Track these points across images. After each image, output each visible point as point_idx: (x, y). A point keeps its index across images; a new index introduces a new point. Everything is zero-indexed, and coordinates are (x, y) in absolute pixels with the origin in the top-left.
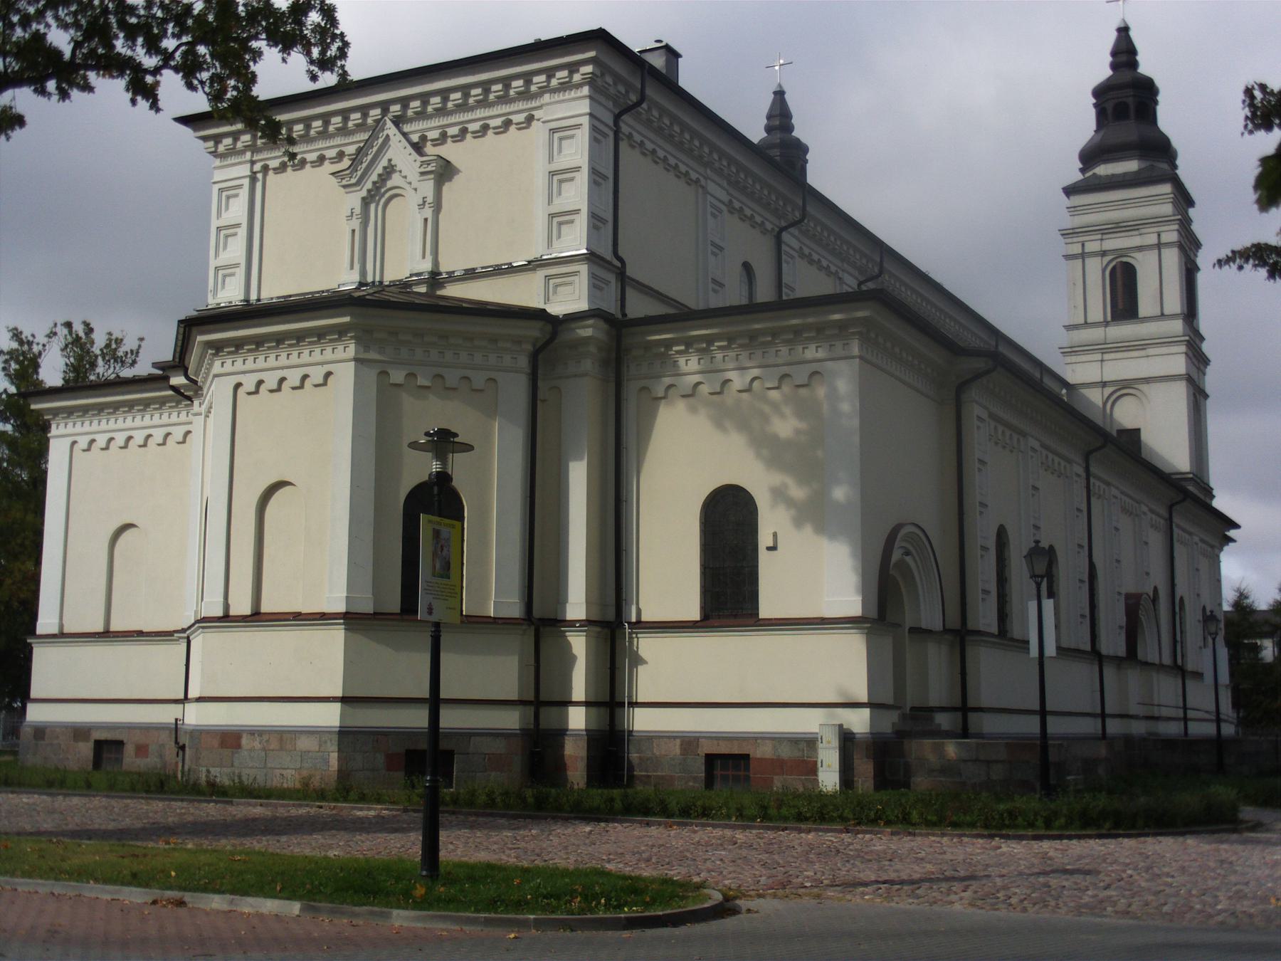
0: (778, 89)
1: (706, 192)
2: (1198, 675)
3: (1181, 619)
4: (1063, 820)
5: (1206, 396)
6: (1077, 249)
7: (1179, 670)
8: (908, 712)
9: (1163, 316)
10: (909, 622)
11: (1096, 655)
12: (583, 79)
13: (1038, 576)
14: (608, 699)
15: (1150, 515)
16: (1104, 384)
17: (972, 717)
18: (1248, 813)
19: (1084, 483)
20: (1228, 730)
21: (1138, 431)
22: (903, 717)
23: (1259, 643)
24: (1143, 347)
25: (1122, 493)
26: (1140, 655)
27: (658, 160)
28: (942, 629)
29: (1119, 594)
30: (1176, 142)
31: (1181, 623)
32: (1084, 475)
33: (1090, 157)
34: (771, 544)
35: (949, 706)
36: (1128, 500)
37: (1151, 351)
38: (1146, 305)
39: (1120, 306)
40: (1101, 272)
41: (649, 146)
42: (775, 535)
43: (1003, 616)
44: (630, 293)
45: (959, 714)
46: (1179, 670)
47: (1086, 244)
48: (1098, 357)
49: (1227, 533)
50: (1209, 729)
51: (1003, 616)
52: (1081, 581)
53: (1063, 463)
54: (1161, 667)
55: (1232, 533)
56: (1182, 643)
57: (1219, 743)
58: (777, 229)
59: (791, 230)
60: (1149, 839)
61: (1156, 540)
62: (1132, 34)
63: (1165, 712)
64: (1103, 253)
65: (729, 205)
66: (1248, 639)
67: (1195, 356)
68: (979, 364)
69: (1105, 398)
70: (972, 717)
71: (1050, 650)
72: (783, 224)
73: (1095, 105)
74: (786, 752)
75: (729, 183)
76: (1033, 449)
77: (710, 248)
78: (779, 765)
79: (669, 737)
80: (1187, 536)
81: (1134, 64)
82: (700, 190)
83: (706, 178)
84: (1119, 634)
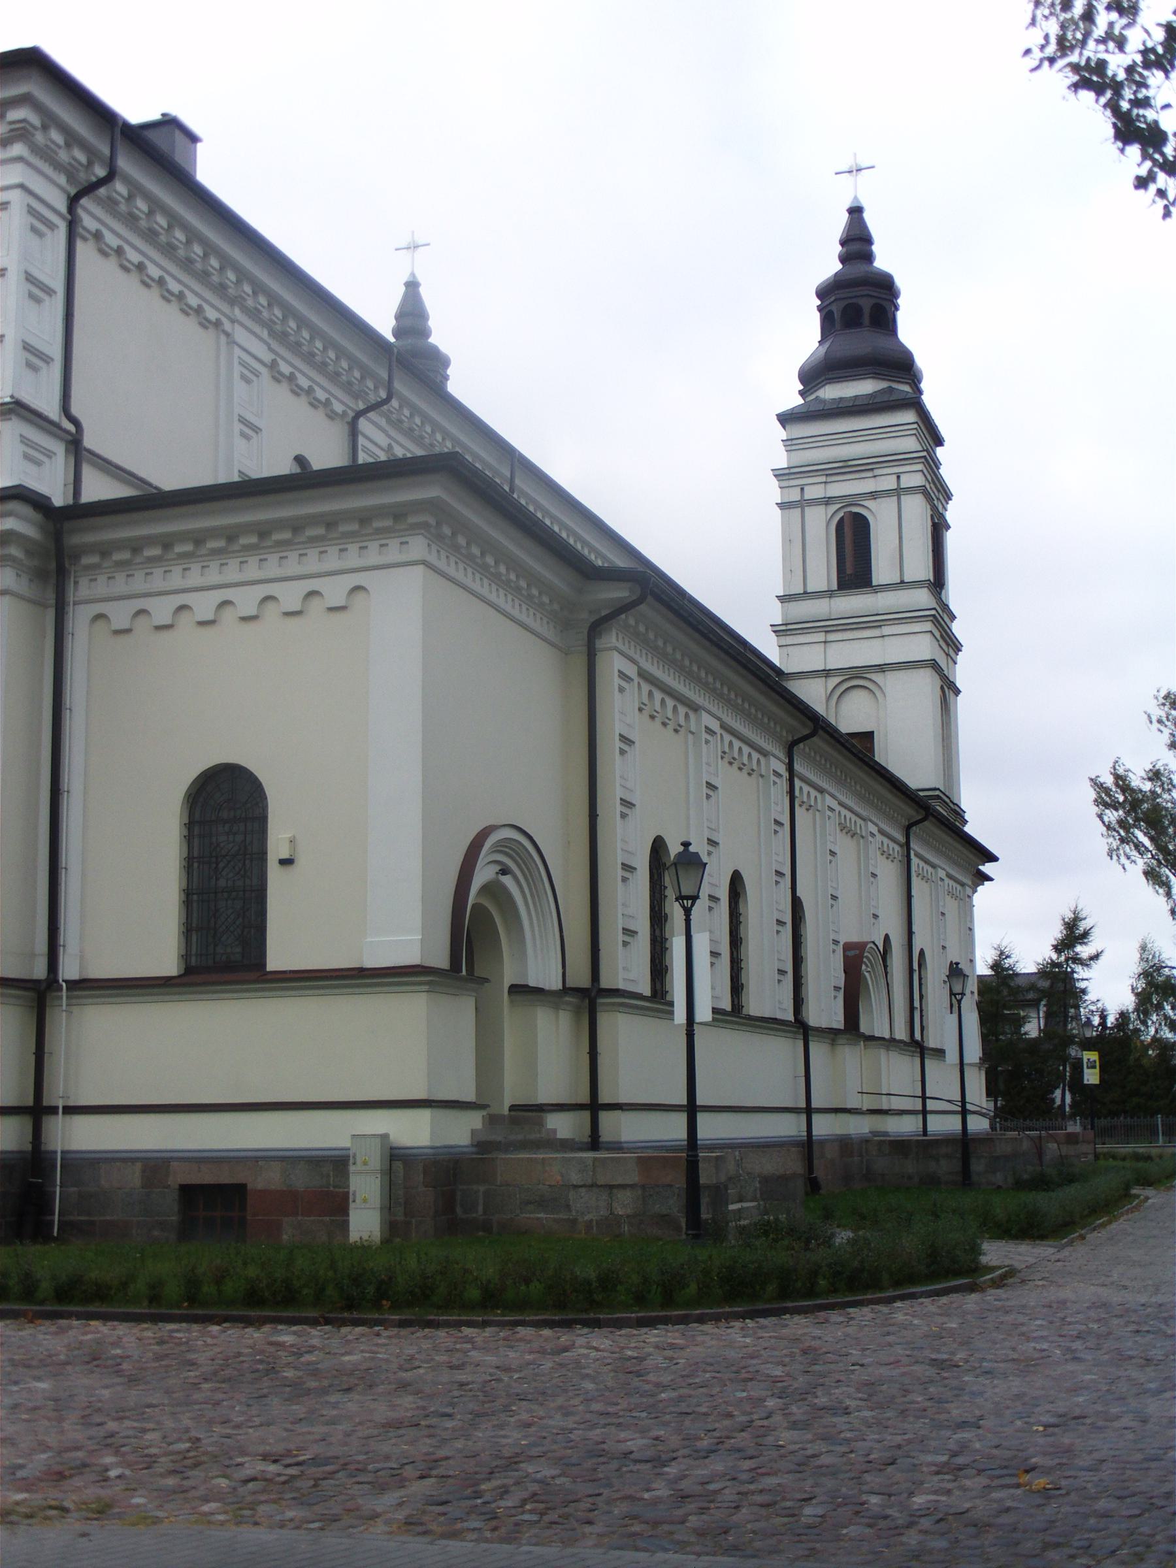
0: (411, 279)
1: (231, 342)
2: (940, 1053)
3: (920, 979)
4: (693, 1288)
5: (957, 692)
6: (795, 495)
7: (918, 1048)
8: (506, 1112)
9: (902, 584)
10: (509, 977)
11: (800, 1028)
12: (12, 130)
13: (688, 898)
14: (30, 1102)
15: (879, 837)
16: (827, 673)
17: (605, 1117)
18: (994, 1253)
19: (783, 785)
20: (978, 1125)
21: (869, 736)
22: (493, 1120)
23: (1022, 1014)
24: (878, 625)
25: (841, 804)
26: (864, 1028)
27: (148, 281)
28: (560, 986)
29: (836, 942)
30: (920, 361)
31: (920, 984)
32: (786, 775)
33: (812, 377)
34: (285, 855)
35: (15, 1104)
36: (849, 815)
37: (886, 630)
38: (882, 571)
39: (849, 570)
40: (825, 525)
41: (134, 257)
42: (292, 841)
43: (659, 969)
44: (87, 472)
45: (586, 1115)
46: (918, 1048)
47: (806, 488)
48: (821, 637)
49: (981, 867)
50: (953, 1124)
51: (659, 969)
52: (780, 923)
53: (813, 793)
54: (891, 1043)
55: (987, 868)
56: (921, 1011)
57: (965, 1142)
58: (351, 414)
59: (371, 415)
60: (835, 1316)
61: (888, 873)
62: (867, 216)
63: (897, 1104)
64: (827, 501)
65: (273, 366)
66: (1009, 1010)
67: (942, 636)
68: (620, 593)
69: (829, 692)
70: (605, 1117)
71: (703, 1013)
72: (361, 406)
73: (820, 309)
74: (301, 1180)
75: (272, 333)
76: (709, 731)
77: (238, 427)
78: (289, 1201)
79: (124, 1160)
80: (930, 869)
81: (869, 257)
82: (223, 338)
83: (233, 321)
84: (835, 997)
